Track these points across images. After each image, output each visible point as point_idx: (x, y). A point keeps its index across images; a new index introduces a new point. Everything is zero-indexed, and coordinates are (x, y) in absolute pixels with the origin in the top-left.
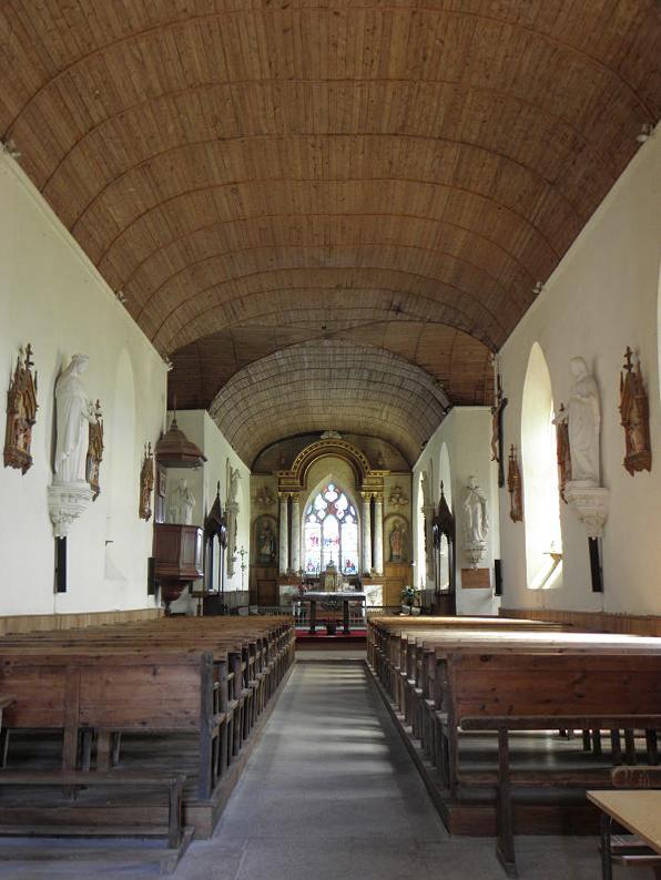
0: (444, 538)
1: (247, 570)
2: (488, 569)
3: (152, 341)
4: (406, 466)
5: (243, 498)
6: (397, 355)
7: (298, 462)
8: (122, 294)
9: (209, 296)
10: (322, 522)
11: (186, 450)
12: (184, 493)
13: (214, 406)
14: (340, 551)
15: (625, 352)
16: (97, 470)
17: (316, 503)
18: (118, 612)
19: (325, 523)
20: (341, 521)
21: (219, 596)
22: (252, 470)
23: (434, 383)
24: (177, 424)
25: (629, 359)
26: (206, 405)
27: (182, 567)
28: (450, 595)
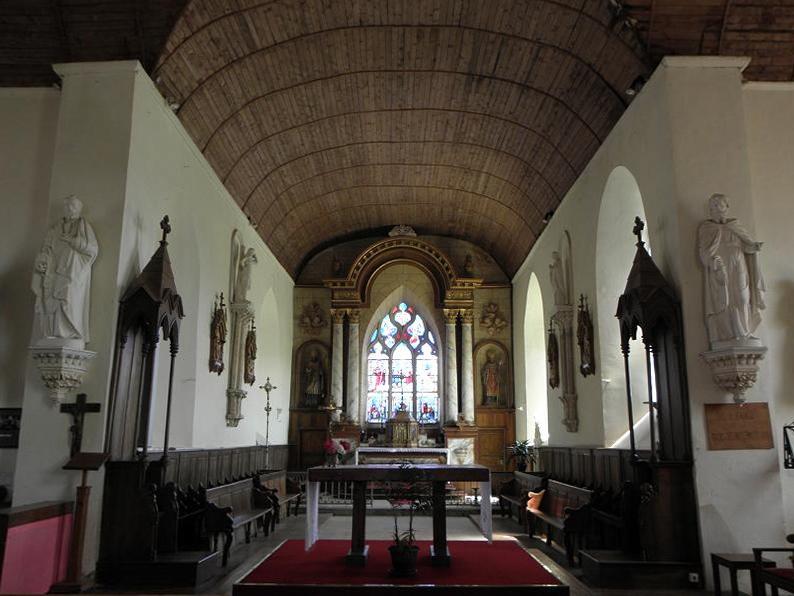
7: (358, 268)
10: (389, 352)
19: (396, 355)
20: (416, 352)
22: (296, 282)
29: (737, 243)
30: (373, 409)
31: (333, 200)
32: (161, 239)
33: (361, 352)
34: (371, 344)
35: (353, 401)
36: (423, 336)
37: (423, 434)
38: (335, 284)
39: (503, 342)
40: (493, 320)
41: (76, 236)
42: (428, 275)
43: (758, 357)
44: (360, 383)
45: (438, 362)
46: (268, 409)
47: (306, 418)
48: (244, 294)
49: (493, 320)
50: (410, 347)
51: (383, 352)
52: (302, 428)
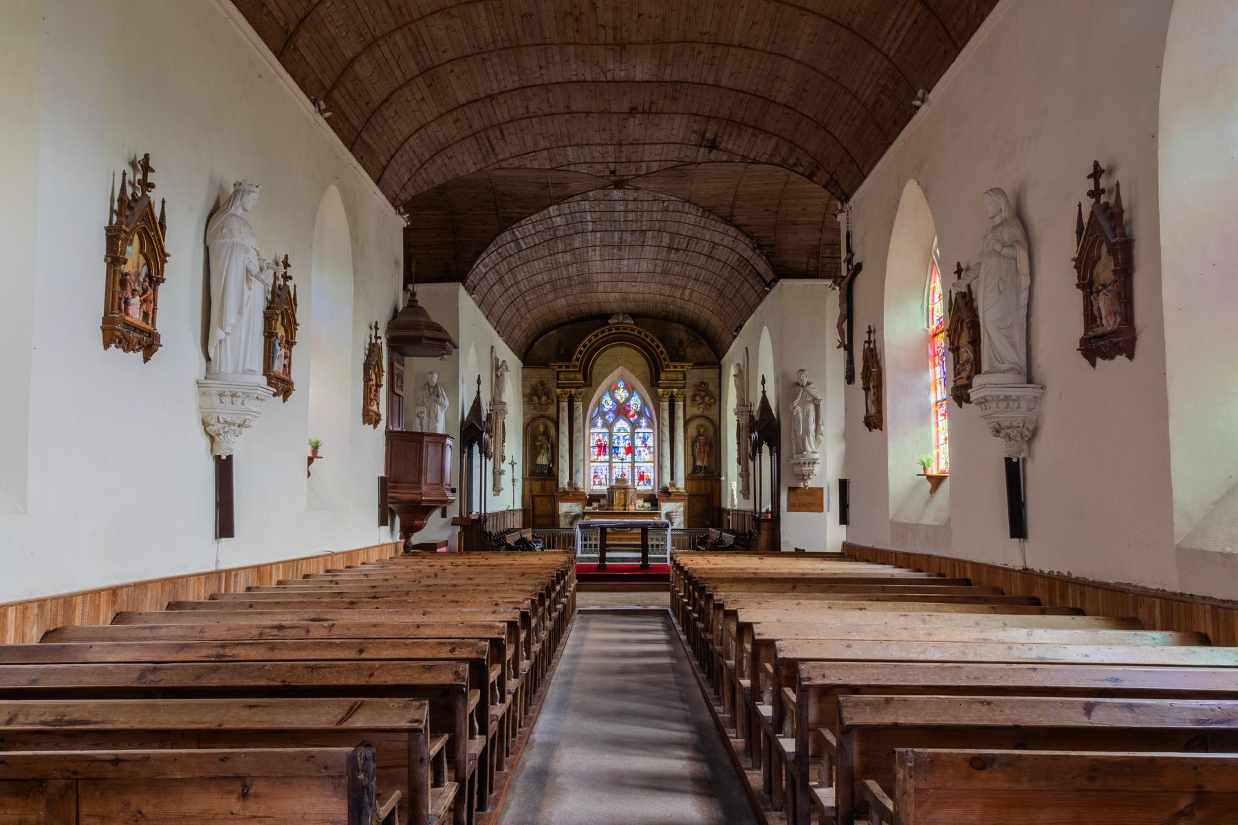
0: (765, 448)
1: (519, 484)
2: (822, 489)
3: (377, 183)
4: (715, 360)
5: (512, 396)
6: (708, 211)
7: (580, 352)
8: (323, 106)
9: (456, 121)
10: (609, 426)
11: (427, 333)
12: (433, 392)
13: (472, 278)
16: (288, 357)
18: (332, 554)
20: (635, 425)
21: (482, 519)
22: (523, 363)
23: (754, 250)
24: (417, 298)
26: (461, 277)
27: (424, 488)
28: (774, 521)
29: (810, 398)
31: (562, 302)
33: (584, 427)
35: (578, 471)
38: (560, 367)
39: (710, 417)
40: (703, 398)
43: (814, 463)
44: (584, 455)
47: (537, 486)
48: (500, 395)
49: (703, 398)
52: (534, 493)
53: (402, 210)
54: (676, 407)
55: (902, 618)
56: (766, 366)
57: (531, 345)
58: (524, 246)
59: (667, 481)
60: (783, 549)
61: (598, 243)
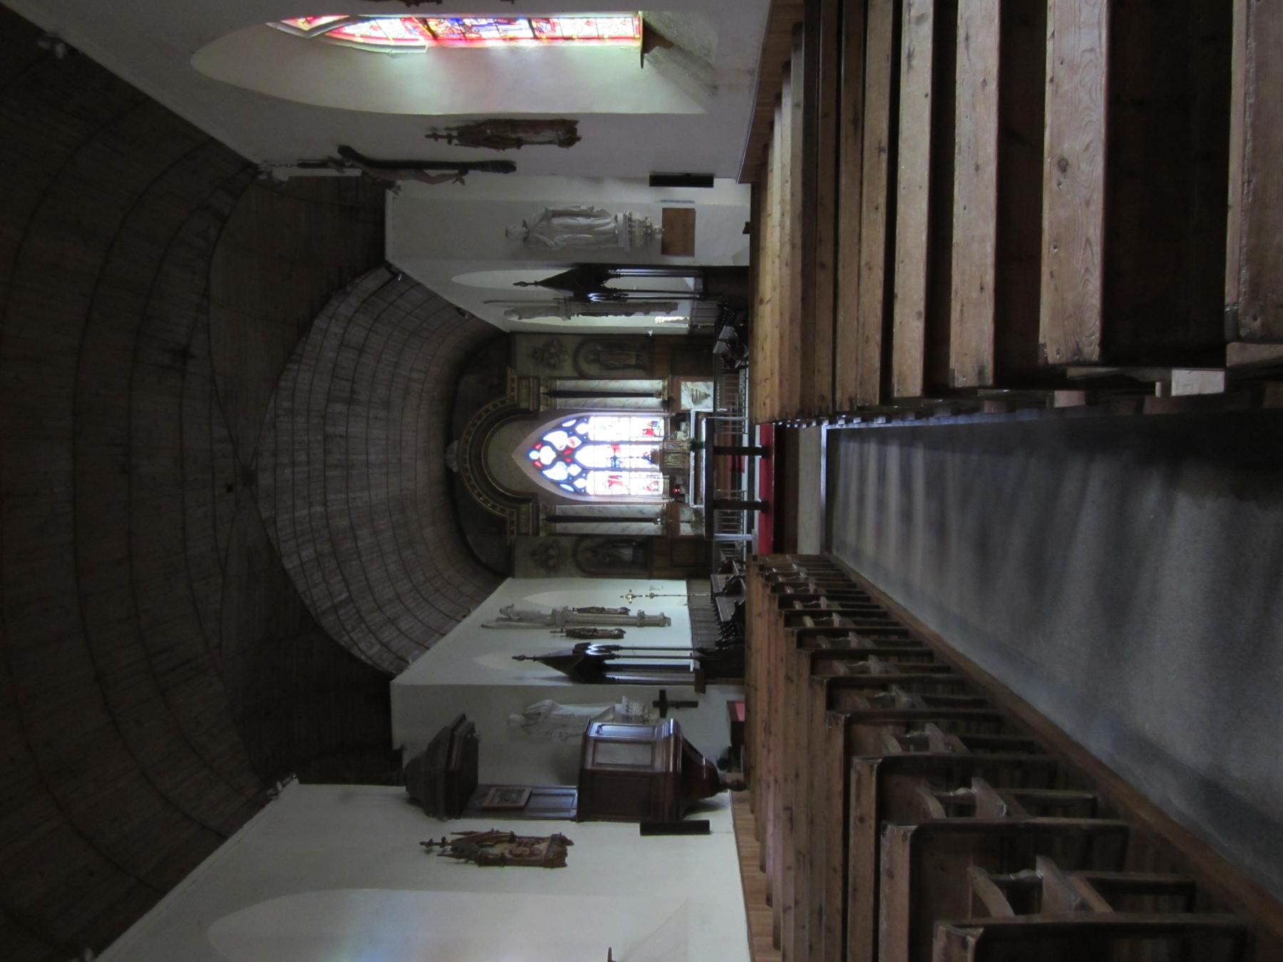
0: (610, 284)
2: (665, 210)
7: (494, 507)
10: (585, 471)
13: (386, 664)
14: (630, 443)
15: (432, 140)
17: (556, 478)
19: (587, 464)
20: (585, 441)
21: (702, 654)
25: (442, 137)
28: (708, 275)
29: (544, 223)
30: (648, 488)
32: (532, 661)
34: (577, 492)
35: (641, 512)
36: (587, 439)
37: (676, 437)
41: (539, 714)
42: (498, 428)
43: (630, 219)
45: (597, 416)
46: (652, 596)
48: (544, 617)
50: (579, 448)
51: (585, 478)
53: (270, 791)
54: (562, 388)
55: (915, 62)
56: (503, 279)
57: (670, 453)
58: (344, 596)
59: (654, 401)
60: (745, 262)
61: (343, 496)
